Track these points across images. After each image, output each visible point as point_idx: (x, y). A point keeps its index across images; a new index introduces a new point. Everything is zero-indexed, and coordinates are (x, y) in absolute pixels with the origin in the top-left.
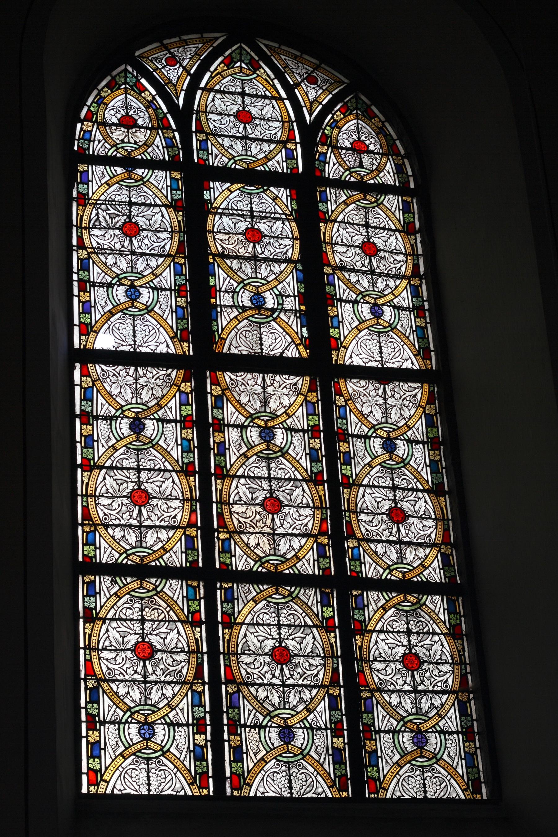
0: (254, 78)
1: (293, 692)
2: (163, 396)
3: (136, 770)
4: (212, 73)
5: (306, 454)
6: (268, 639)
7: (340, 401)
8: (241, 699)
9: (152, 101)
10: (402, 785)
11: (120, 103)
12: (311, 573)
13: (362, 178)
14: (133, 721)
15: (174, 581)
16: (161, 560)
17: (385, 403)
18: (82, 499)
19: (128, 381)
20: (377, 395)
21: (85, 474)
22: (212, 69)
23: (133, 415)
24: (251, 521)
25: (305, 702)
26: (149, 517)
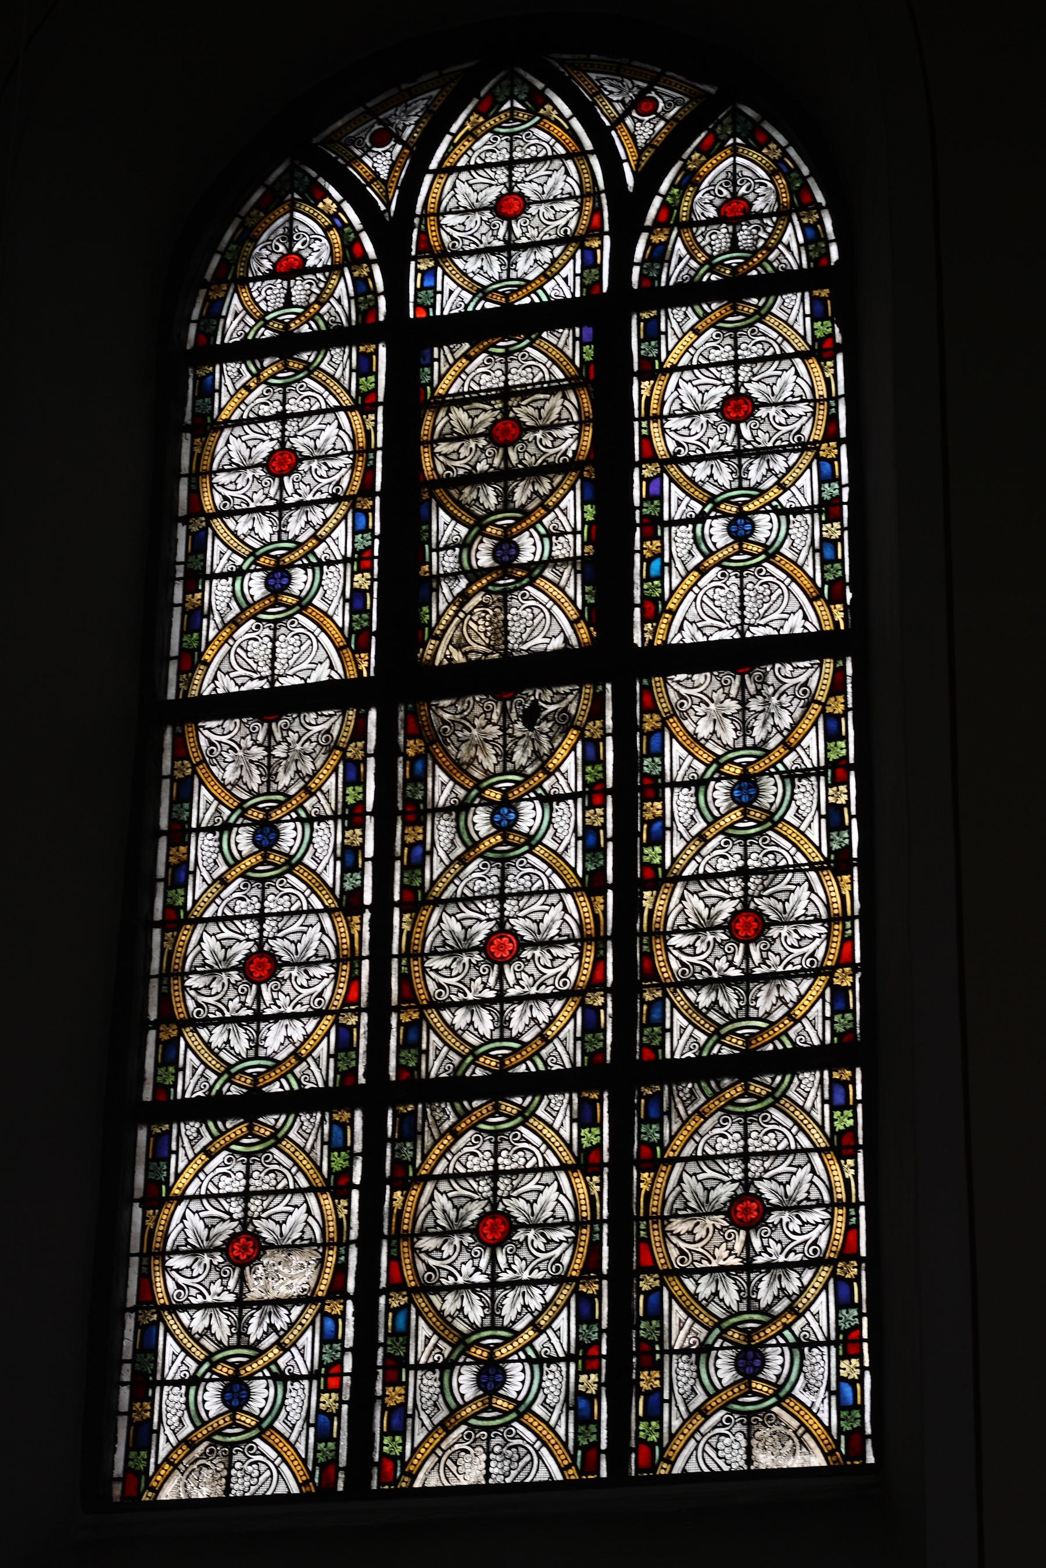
0: (535, 126)
1: (766, 1279)
2: (316, 772)
3: (727, 1436)
4: (454, 135)
5: (821, 817)
6: (724, 1182)
7: (651, 722)
8: (413, 1317)
9: (336, 215)
10: (704, 1451)
11: (724, 175)
12: (816, 1042)
13: (287, 325)
14: (726, 1344)
15: (807, 1075)
16: (784, 1039)
17: (270, 756)
18: (400, 962)
19: (491, 733)
20: (489, 722)
21: (407, 917)
22: (454, 129)
23: (738, 771)
24: (219, 1001)
25: (789, 1297)
26: (764, 961)
